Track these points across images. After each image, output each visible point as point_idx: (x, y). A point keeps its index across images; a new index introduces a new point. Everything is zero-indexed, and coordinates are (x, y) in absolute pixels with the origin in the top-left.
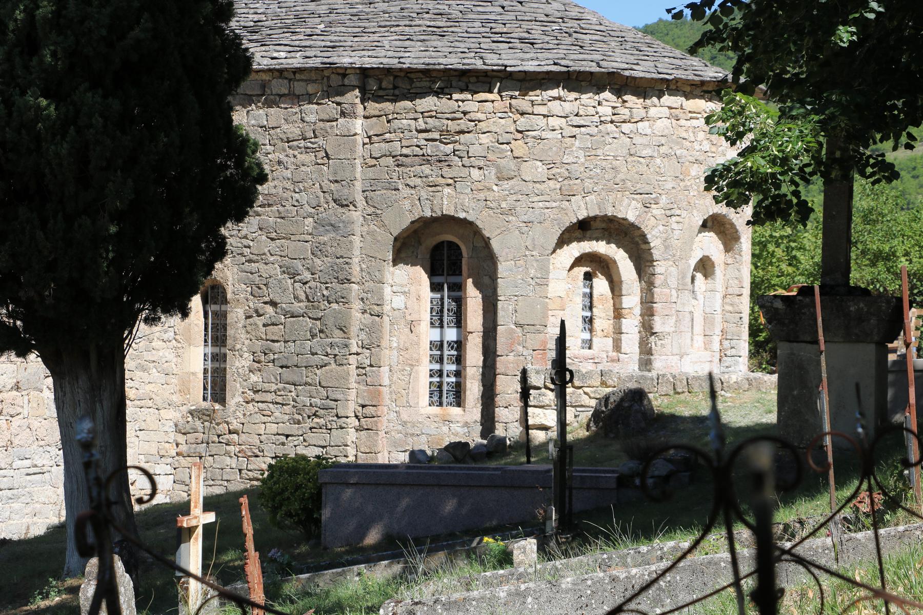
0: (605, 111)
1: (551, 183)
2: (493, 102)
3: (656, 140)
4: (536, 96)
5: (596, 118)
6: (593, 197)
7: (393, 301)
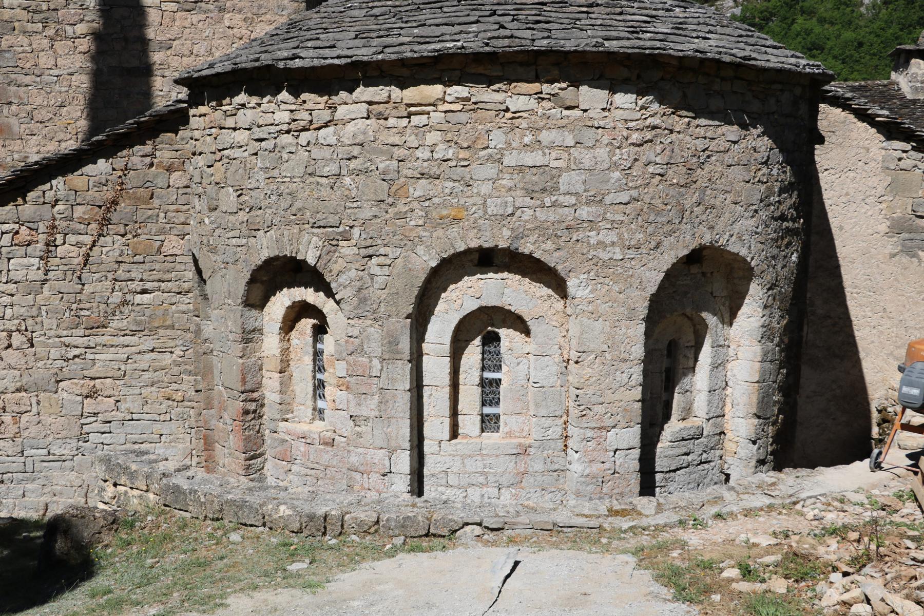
3: (343, 152)
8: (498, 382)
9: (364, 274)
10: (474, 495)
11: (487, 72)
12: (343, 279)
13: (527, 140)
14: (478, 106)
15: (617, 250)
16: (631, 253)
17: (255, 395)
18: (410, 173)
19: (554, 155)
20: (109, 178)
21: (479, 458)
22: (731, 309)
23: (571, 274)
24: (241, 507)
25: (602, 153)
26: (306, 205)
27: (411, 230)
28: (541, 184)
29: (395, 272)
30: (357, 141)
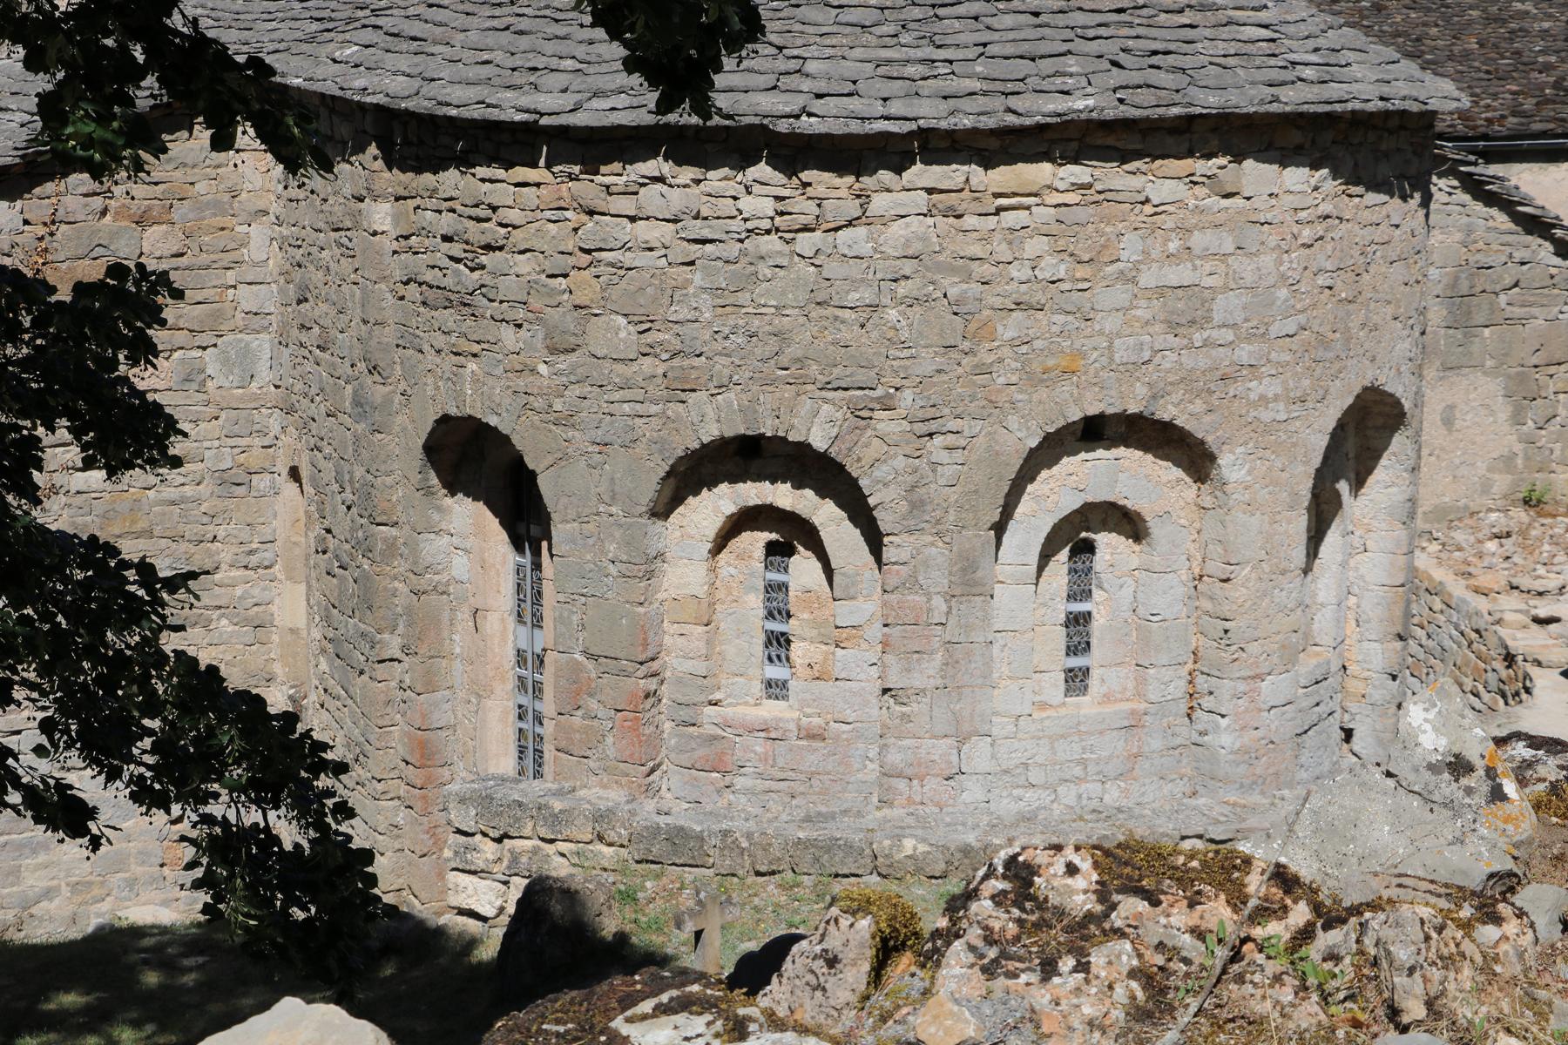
0: (759, 205)
1: (648, 360)
2: (538, 185)
3: (884, 268)
4: (614, 175)
5: (737, 225)
6: (732, 395)
7: (292, 605)
8: (1087, 616)
9: (922, 464)
10: (1068, 794)
11: (1119, 145)
12: (881, 472)
13: (1173, 246)
14: (1107, 196)
15: (1281, 406)
16: (1296, 411)
17: (655, 666)
18: (998, 302)
19: (1208, 268)
20: (18, 239)
21: (1076, 738)
22: (1357, 474)
23: (1225, 447)
24: (828, 850)
25: (1267, 260)
26: (810, 354)
27: (999, 391)
28: (1186, 313)
29: (974, 457)
30: (910, 253)
